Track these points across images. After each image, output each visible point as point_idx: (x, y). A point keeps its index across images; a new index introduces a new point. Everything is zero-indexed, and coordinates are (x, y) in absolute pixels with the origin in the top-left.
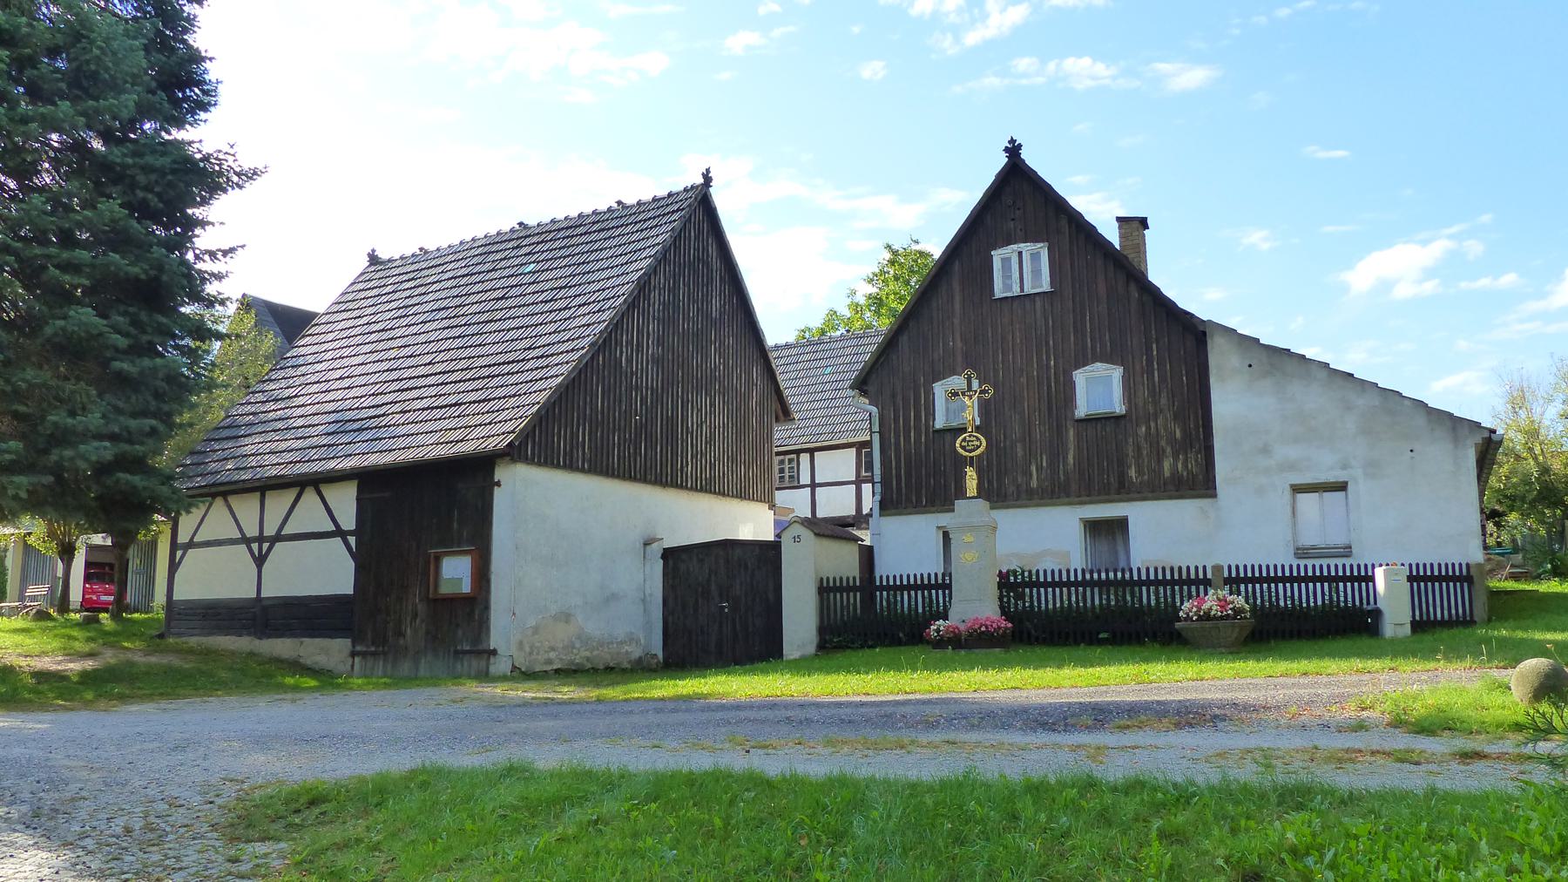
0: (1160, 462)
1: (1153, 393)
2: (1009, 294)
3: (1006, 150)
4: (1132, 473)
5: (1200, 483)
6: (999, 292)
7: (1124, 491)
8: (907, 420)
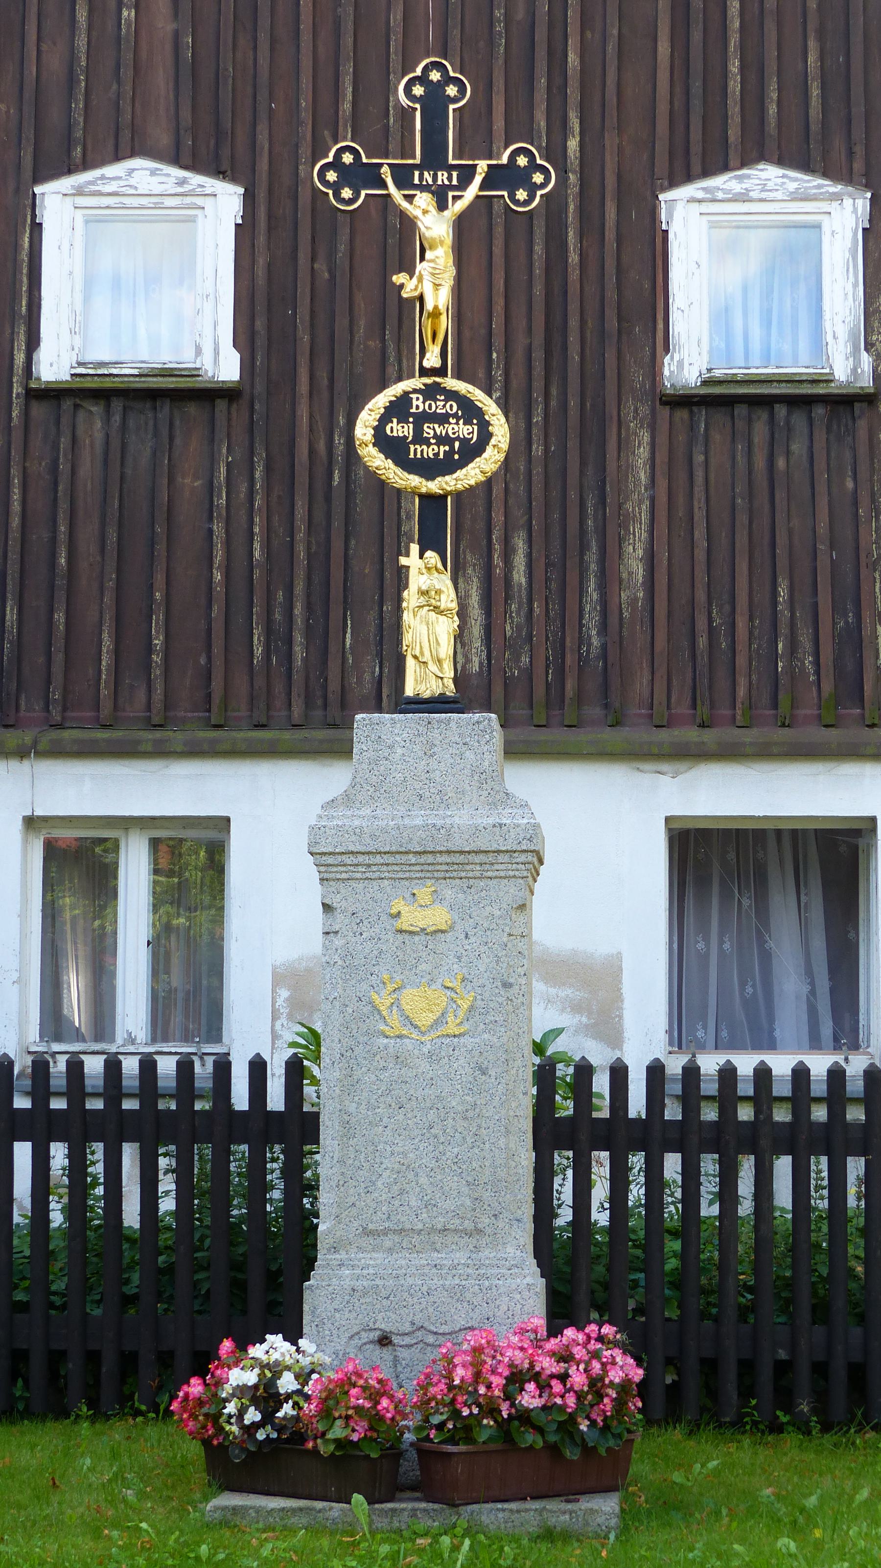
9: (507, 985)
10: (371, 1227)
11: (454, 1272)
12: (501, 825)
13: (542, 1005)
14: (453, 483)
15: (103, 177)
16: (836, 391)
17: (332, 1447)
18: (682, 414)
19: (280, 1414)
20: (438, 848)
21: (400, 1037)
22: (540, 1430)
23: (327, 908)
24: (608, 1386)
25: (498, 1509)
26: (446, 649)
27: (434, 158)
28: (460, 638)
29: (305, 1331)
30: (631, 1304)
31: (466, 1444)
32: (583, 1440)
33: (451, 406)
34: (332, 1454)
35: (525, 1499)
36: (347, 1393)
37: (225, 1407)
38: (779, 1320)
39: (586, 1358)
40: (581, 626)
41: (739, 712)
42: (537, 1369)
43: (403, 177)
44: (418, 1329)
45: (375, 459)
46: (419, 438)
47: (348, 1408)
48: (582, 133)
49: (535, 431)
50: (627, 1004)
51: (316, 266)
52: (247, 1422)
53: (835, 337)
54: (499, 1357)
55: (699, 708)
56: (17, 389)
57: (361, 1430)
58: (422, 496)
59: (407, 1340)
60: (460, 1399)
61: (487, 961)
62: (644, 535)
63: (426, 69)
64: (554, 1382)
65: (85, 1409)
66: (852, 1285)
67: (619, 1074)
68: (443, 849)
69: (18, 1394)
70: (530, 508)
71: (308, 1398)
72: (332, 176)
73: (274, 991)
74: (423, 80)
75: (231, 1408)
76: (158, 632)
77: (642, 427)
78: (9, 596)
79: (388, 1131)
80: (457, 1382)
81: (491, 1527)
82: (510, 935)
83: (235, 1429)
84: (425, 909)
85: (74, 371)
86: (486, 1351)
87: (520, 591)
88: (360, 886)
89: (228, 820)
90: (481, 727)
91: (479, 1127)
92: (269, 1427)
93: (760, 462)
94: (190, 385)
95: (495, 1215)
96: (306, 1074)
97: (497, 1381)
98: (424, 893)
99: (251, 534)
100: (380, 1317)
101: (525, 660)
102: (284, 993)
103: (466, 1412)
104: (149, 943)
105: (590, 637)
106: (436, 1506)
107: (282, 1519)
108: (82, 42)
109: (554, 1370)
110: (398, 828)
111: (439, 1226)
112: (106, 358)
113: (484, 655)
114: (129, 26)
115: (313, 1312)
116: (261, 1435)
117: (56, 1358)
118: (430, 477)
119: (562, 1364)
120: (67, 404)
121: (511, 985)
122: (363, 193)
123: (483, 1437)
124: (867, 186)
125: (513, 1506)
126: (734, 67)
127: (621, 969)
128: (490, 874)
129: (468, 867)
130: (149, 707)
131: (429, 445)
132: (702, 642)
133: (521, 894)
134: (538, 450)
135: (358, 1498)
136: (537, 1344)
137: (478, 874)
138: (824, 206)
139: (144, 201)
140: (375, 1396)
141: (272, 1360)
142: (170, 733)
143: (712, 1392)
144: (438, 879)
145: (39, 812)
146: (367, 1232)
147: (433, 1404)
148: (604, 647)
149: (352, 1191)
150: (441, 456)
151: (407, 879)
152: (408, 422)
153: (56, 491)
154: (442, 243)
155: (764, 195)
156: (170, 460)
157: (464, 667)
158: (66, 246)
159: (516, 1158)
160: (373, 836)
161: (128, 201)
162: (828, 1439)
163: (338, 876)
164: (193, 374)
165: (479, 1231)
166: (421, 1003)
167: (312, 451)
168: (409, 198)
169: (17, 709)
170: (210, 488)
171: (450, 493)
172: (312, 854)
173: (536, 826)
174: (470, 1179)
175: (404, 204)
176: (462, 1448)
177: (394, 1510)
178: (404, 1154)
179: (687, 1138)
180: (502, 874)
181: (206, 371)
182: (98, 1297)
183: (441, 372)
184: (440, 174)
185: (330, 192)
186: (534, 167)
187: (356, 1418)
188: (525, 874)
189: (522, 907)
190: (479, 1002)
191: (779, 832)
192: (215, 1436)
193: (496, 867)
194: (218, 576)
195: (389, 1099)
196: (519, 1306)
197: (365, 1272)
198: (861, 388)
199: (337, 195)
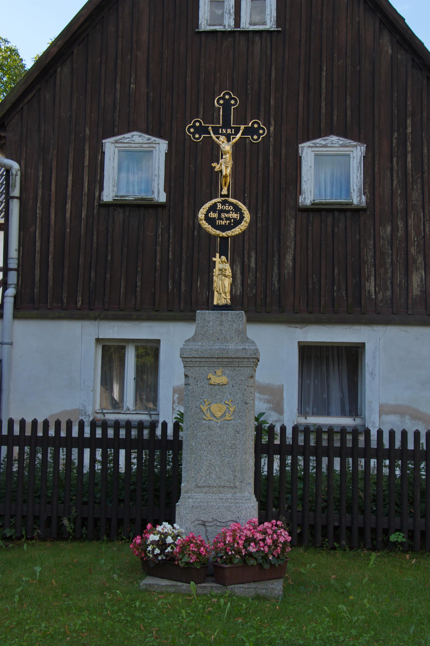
0: (407, 274)
2: (218, 28)
4: (370, 286)
9: (246, 403)
10: (199, 485)
11: (227, 501)
12: (245, 349)
13: (258, 401)
14: (231, 233)
15: (124, 138)
16: (354, 207)
17: (184, 564)
18: (305, 214)
19: (166, 551)
20: (224, 356)
21: (210, 420)
22: (256, 559)
23: (186, 376)
24: (279, 543)
25: (241, 587)
26: (228, 289)
27: (226, 125)
28: (232, 285)
29: (176, 520)
30: (286, 506)
31: (230, 564)
32: (270, 562)
33: (231, 208)
34: (184, 567)
35: (250, 582)
36: (189, 545)
37: (148, 548)
38: (335, 512)
39: (272, 533)
40: (272, 280)
41: (322, 309)
42: (255, 537)
43: (216, 131)
44: (215, 520)
45: (205, 225)
46: (220, 218)
47: (189, 551)
48: (275, 125)
49: (258, 219)
50: (285, 401)
51: (190, 166)
52: (155, 553)
53: (354, 190)
54: (242, 533)
55: (309, 307)
56: (96, 204)
57: (194, 559)
58: (220, 238)
59: (211, 524)
60: (228, 548)
61: (240, 395)
62: (292, 252)
63: (224, 95)
64: (261, 542)
65: (105, 538)
66: (360, 501)
67: (283, 429)
68: (225, 357)
69: (84, 532)
70: (257, 243)
71: (176, 545)
72: (192, 130)
73: (173, 395)
74: (223, 98)
75: (150, 548)
76: (139, 281)
77: (292, 218)
78: (92, 269)
79: (205, 452)
80: (227, 542)
81: (238, 593)
82: (248, 386)
83: (151, 556)
84: (219, 378)
85: (114, 198)
86: (238, 531)
87: (253, 269)
88: (197, 369)
89: (160, 340)
90: (239, 316)
91: (236, 451)
92: (162, 555)
93: (329, 230)
94: (150, 203)
95: (241, 482)
96: (180, 428)
97: (241, 542)
98: (219, 372)
99: (169, 250)
100: (202, 516)
101: (254, 291)
102: (177, 396)
103: (230, 553)
104: (134, 378)
105: (275, 284)
106: (219, 585)
107: (166, 589)
108: (118, 95)
109: (261, 538)
110: (210, 349)
111: (222, 485)
112: (124, 194)
113: (241, 290)
114: (133, 90)
115: (179, 514)
116: (160, 558)
117: (96, 520)
118: (223, 231)
119: (263, 535)
120: (112, 209)
121: (248, 403)
122: (202, 136)
123: (236, 561)
124: (365, 143)
125: (246, 586)
126: (323, 104)
127: (283, 390)
128: (241, 365)
129: (234, 363)
130: (135, 304)
131: (223, 220)
132: (310, 286)
133: (252, 372)
134: (259, 225)
135: (192, 583)
136: (255, 528)
137: (237, 365)
138: (351, 149)
139: (137, 145)
140: (199, 546)
141: (164, 532)
142: (142, 313)
143: (313, 535)
144: (223, 367)
145: (100, 337)
146: (198, 487)
147: (219, 549)
148: (279, 288)
149: (193, 472)
150: (227, 224)
151: (213, 367)
152: (216, 213)
153: (108, 236)
154: (228, 153)
155: (332, 145)
156: (143, 227)
157: (235, 293)
158: (112, 159)
159: (249, 462)
160: (202, 352)
161: (132, 145)
162: (352, 553)
163: (190, 365)
164: (151, 200)
165: (236, 487)
166: (217, 409)
167: (188, 224)
168: (218, 138)
169: (94, 305)
170: (156, 236)
171: (230, 236)
172: (181, 357)
173: (257, 350)
174: (233, 469)
175: (216, 140)
176: (229, 566)
177: (205, 587)
178: (211, 460)
179: (305, 451)
180: (245, 365)
181: (155, 199)
182: (111, 500)
183: (227, 196)
184: (228, 130)
185: (191, 135)
186: (260, 128)
187: (192, 554)
188: (253, 365)
189: (252, 377)
190: (237, 409)
191: (333, 347)
192: (145, 557)
193: (243, 363)
194: (158, 263)
195: (206, 441)
196: (249, 513)
197: (197, 500)
198: (362, 207)
199: (194, 137)
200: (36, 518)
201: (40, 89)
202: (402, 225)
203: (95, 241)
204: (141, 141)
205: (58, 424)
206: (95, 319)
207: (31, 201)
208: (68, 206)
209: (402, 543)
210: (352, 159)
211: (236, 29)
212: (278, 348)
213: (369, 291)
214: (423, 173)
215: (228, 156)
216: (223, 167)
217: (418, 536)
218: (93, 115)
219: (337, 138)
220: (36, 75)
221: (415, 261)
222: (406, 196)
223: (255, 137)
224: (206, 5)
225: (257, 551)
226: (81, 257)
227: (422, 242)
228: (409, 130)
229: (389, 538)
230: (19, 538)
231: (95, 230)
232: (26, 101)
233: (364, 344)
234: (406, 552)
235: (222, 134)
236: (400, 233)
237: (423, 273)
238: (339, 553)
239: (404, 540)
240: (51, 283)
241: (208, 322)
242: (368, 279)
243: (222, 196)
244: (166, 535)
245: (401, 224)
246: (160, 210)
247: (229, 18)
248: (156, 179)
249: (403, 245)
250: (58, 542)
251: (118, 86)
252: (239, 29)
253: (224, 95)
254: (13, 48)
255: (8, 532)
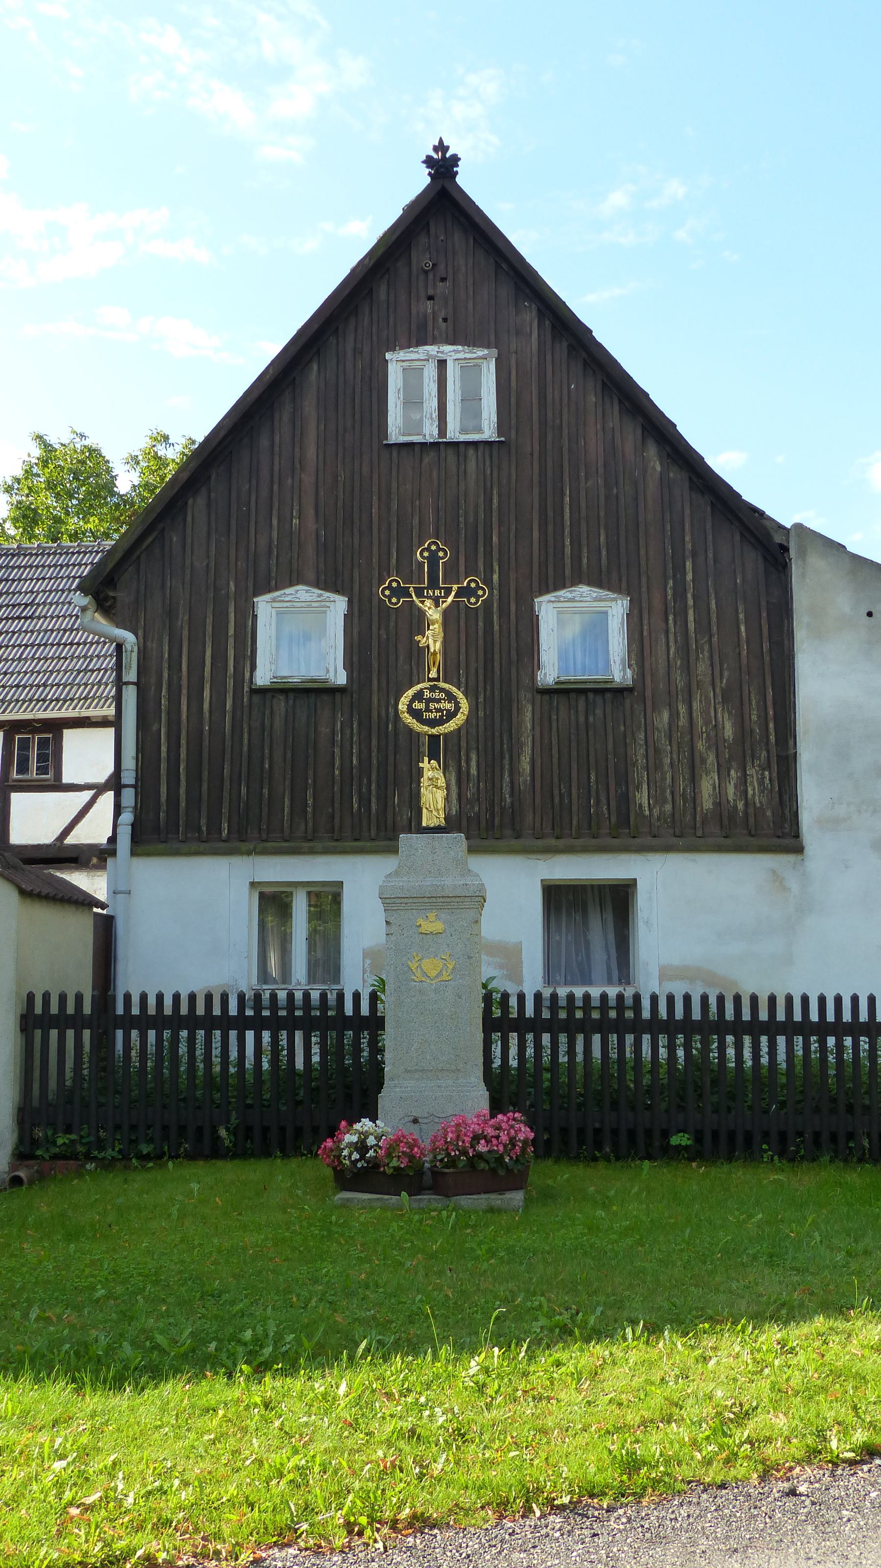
0: (694, 780)
1: (685, 650)
3: (429, 161)
4: (642, 797)
5: (773, 828)
6: (396, 430)
7: (627, 831)
8: (196, 665)
9: (470, 957)
10: (409, 1069)
15: (285, 594)
17: (392, 1170)
18: (546, 697)
22: (487, 1162)
26: (441, 804)
27: (433, 584)
28: (447, 799)
30: (528, 1103)
40: (502, 793)
43: (419, 593)
45: (408, 719)
46: (428, 710)
56: (246, 689)
58: (429, 735)
66: (629, 1093)
71: (380, 1148)
75: (345, 1153)
83: (347, 1162)
84: (432, 924)
88: (402, 913)
93: (582, 719)
97: (467, 1139)
98: (432, 915)
99: (352, 753)
101: (477, 809)
102: (368, 962)
103: (453, 1154)
108: (275, 534)
116: (359, 1165)
117: (265, 1130)
120: (269, 696)
123: (461, 1165)
124: (628, 594)
125: (475, 1197)
126: (567, 542)
132: (557, 800)
134: (481, 714)
138: (608, 604)
139: (303, 604)
146: (407, 1071)
148: (512, 803)
154: (437, 622)
162: (619, 1164)
164: (325, 681)
167: (379, 715)
173: (483, 885)
175: (421, 605)
176: (452, 1170)
177: (420, 1199)
183: (437, 679)
189: (477, 922)
191: (592, 886)
194: (337, 772)
200: (182, 1129)
201: (164, 528)
202: (684, 710)
203: (246, 741)
204: (309, 599)
205: (209, 998)
206: (249, 853)
207: (153, 688)
208: (207, 693)
209: (686, 1148)
210: (610, 618)
211: (441, 440)
212: (511, 892)
213: (640, 805)
214: (711, 636)
215: (436, 626)
216: (431, 641)
217: (708, 1138)
218: (239, 563)
219: (589, 589)
220: (159, 510)
221: (703, 761)
222: (688, 669)
223: (473, 600)
224: (398, 408)
225: (489, 1151)
226: (226, 766)
227: (712, 734)
228: (689, 577)
229: (669, 1141)
230: (160, 1156)
231: (245, 726)
232: (144, 547)
233: (635, 880)
234: (693, 1160)
235: (429, 597)
236: (683, 722)
237: (716, 778)
238: (602, 1164)
239: (689, 1143)
240: (183, 804)
241: (416, 849)
242: (638, 787)
243: (430, 680)
244: (366, 1135)
245: (682, 709)
246: (338, 695)
247: (432, 425)
248: (332, 651)
249: (687, 738)
250: (213, 1161)
251: (275, 522)
252: (445, 440)
253: (429, 545)
254: (94, 446)
255: (145, 1149)
